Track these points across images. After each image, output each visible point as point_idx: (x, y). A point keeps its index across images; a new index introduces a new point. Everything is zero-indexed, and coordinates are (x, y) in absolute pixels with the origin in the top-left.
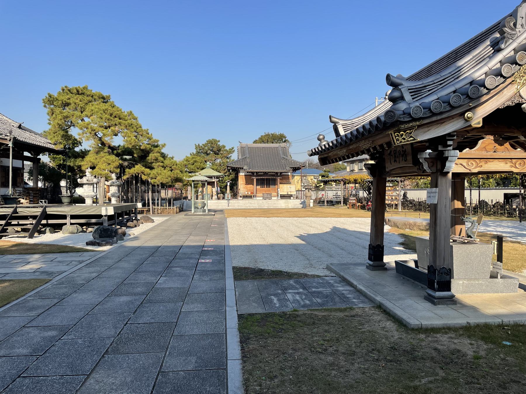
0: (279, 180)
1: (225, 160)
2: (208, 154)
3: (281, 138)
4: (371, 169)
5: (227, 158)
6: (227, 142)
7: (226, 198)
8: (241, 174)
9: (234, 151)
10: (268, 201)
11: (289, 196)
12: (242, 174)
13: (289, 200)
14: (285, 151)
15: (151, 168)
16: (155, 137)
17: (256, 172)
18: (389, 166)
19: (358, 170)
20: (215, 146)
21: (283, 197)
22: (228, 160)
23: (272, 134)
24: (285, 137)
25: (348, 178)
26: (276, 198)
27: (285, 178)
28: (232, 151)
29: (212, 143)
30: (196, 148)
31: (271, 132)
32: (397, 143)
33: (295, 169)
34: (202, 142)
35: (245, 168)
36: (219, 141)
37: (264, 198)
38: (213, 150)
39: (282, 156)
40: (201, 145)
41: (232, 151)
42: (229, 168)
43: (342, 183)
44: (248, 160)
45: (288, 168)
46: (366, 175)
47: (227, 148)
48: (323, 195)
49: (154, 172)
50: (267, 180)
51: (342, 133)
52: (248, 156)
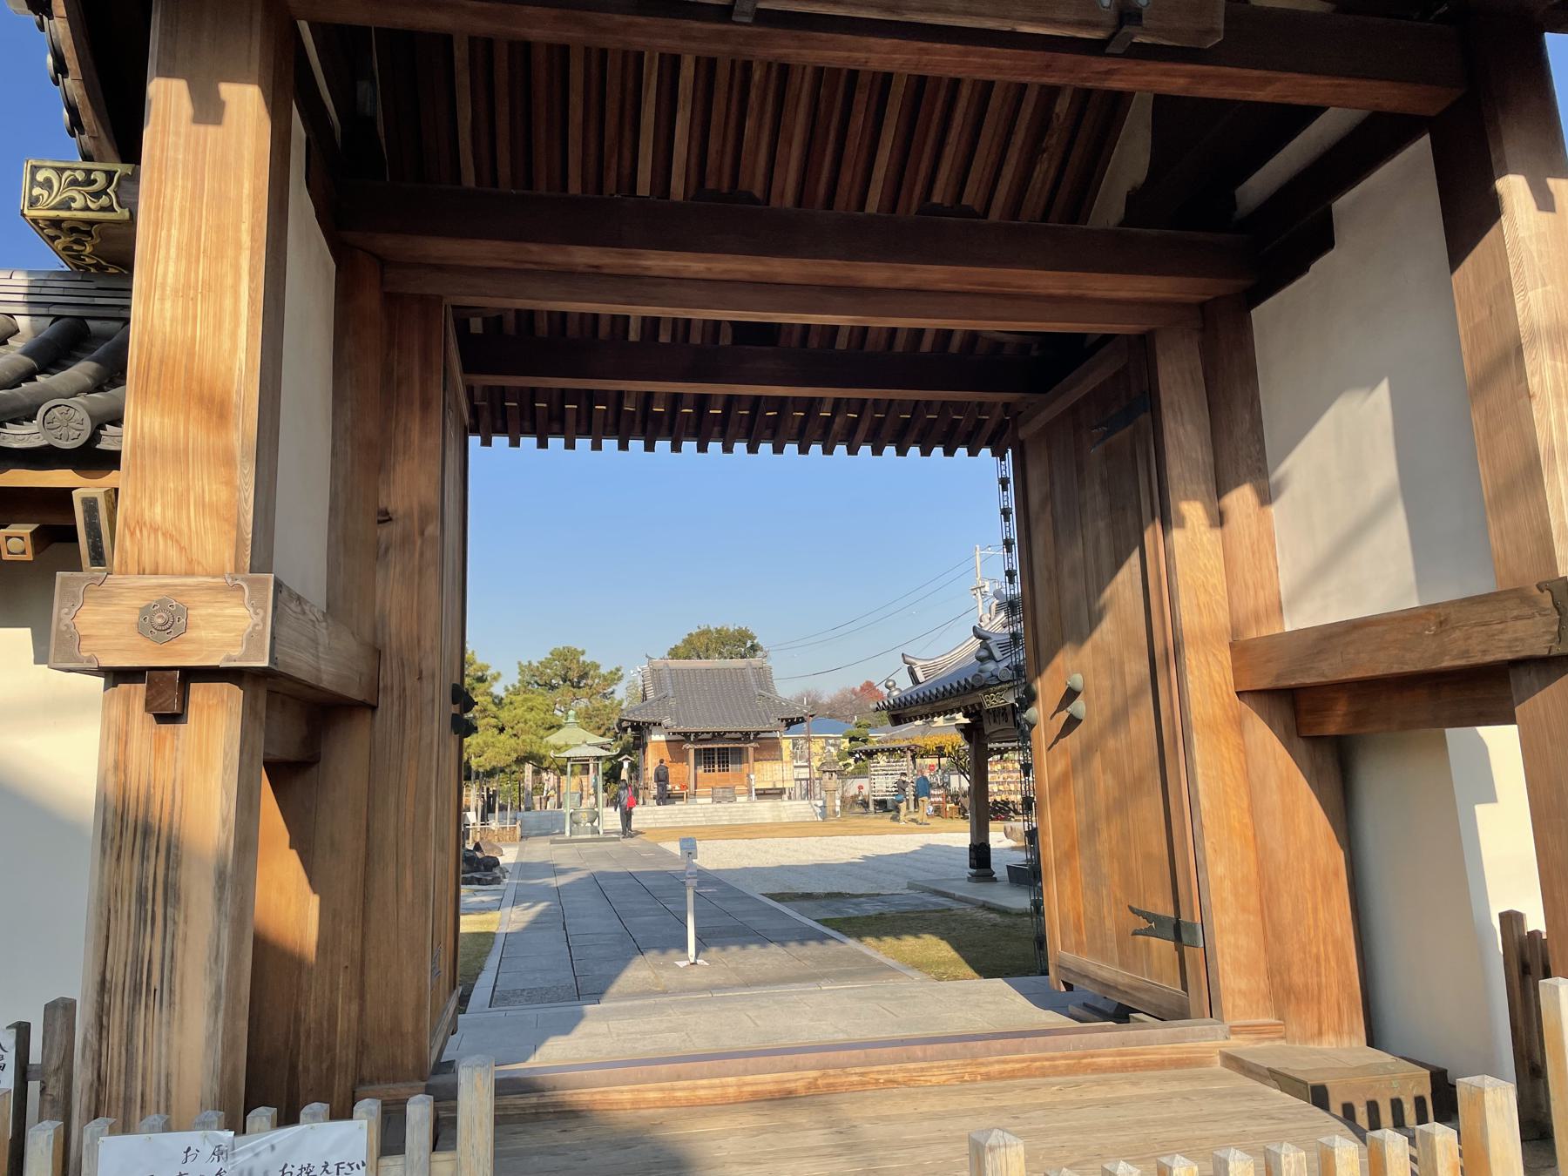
0: (751, 751)
1: (597, 702)
2: (553, 688)
3: (741, 643)
4: (966, 731)
6: (599, 655)
9: (620, 679)
10: (725, 805)
11: (777, 793)
12: (657, 737)
13: (778, 802)
17: (697, 734)
18: (989, 728)
19: (946, 729)
20: (574, 666)
21: (762, 794)
22: (607, 702)
23: (718, 631)
24: (752, 638)
25: (921, 743)
26: (744, 799)
27: (768, 747)
28: (615, 677)
29: (566, 656)
30: (522, 672)
32: (988, 707)
33: (790, 723)
35: (667, 721)
36: (583, 653)
37: (717, 800)
38: (569, 676)
40: (535, 664)
41: (615, 677)
42: (624, 724)
43: (909, 754)
44: (672, 703)
46: (959, 739)
47: (603, 671)
48: (861, 787)
50: (720, 752)
51: (921, 678)
52: (671, 693)
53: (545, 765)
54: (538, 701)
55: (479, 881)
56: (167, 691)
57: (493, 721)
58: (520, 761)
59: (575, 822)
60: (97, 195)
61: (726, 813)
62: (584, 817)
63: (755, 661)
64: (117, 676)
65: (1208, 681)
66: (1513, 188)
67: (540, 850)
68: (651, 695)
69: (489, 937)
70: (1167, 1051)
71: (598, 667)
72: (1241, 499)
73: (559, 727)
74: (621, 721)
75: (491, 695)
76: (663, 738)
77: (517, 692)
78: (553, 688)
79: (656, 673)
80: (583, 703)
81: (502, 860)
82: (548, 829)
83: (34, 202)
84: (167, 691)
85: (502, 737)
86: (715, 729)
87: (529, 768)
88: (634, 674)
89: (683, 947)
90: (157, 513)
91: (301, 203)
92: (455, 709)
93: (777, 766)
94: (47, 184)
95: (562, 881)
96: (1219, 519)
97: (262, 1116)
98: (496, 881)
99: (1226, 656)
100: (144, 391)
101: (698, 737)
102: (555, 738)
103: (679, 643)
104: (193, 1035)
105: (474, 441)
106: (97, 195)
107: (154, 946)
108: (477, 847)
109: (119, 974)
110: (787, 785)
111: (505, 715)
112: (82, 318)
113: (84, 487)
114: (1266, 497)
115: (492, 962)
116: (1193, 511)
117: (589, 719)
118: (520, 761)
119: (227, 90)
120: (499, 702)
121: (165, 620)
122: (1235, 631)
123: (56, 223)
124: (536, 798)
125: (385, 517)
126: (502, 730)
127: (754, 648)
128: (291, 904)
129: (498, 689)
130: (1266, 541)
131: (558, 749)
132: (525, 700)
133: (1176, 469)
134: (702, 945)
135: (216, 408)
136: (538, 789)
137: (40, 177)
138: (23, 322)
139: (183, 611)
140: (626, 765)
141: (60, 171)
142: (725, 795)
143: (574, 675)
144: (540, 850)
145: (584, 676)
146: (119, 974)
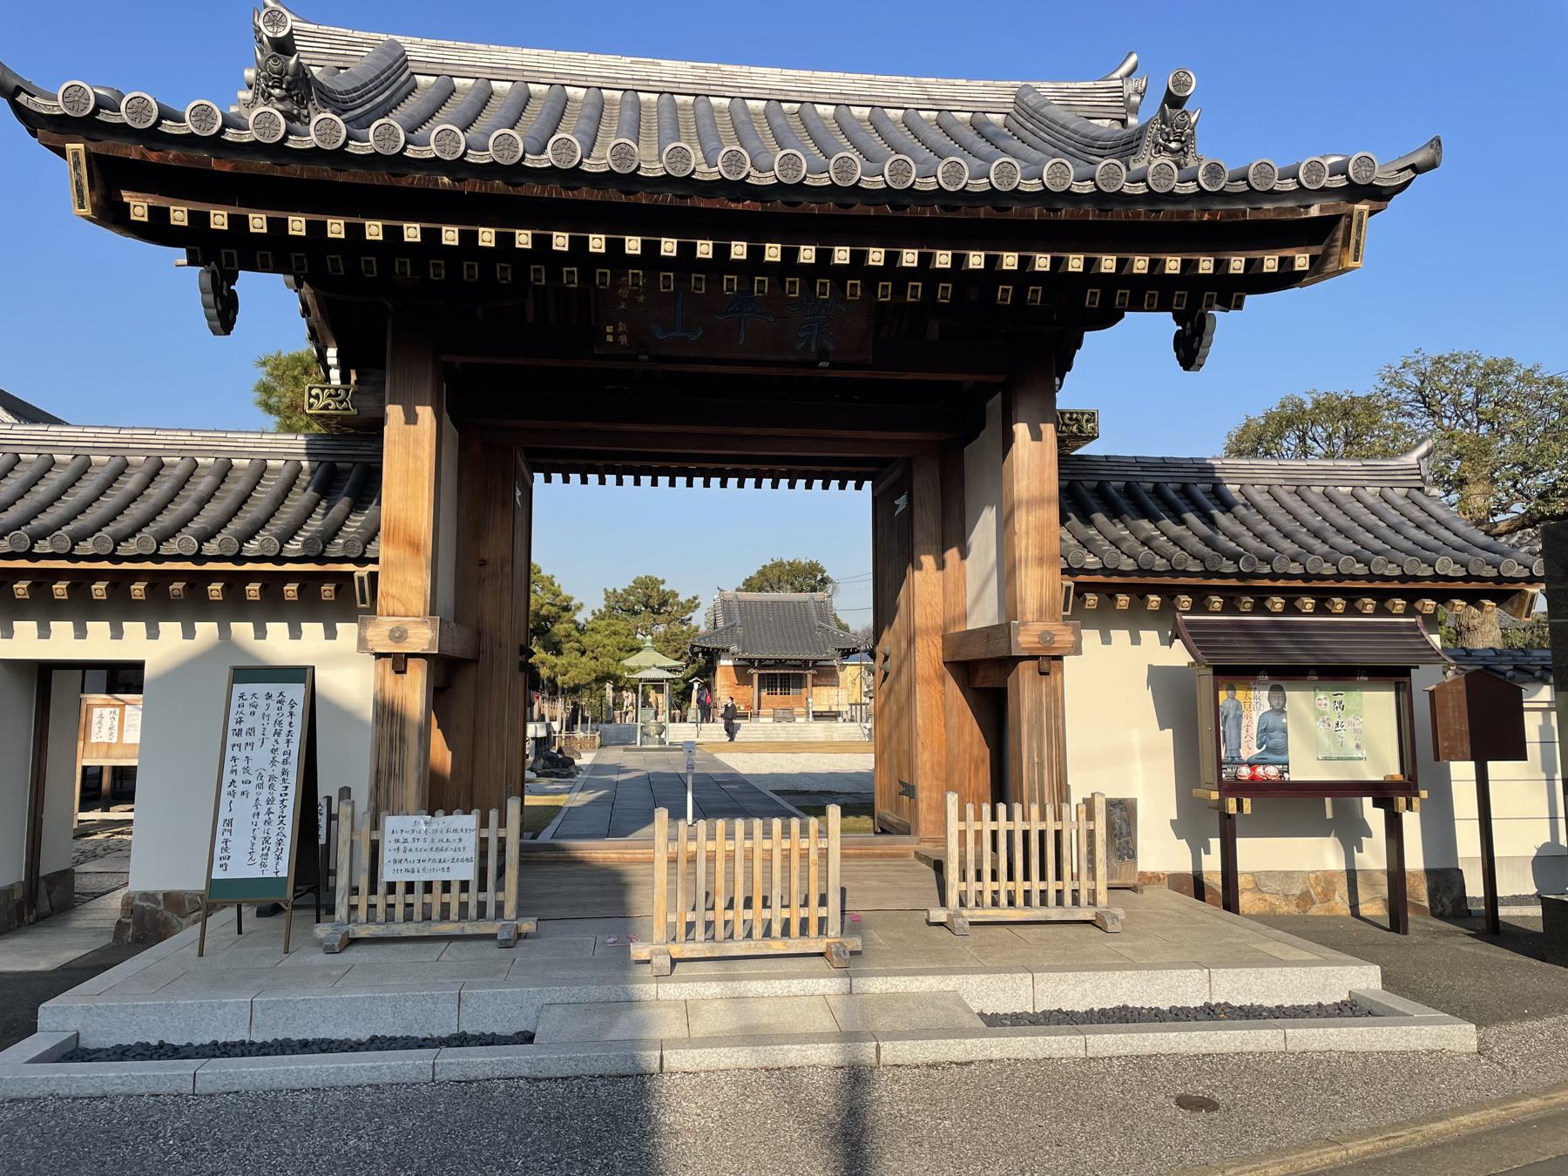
0: (809, 677)
1: (676, 628)
2: (636, 613)
5: (682, 622)
7: (689, 718)
8: (723, 662)
9: (697, 606)
10: (784, 724)
11: (833, 716)
12: (725, 663)
13: (833, 724)
14: (824, 610)
15: (559, 653)
16: (565, 592)
21: (818, 716)
26: (802, 720)
27: (826, 674)
28: (693, 604)
30: (607, 598)
31: (788, 558)
33: (846, 653)
34: (622, 583)
37: (777, 720)
38: (649, 602)
39: (818, 623)
40: (619, 591)
41: (693, 604)
44: (740, 631)
45: (831, 651)
47: (682, 599)
49: (561, 661)
50: (783, 676)
53: (621, 684)
54: (620, 626)
55: (558, 775)
56: (400, 663)
57: (576, 645)
58: (601, 679)
59: (644, 734)
60: (341, 402)
61: (783, 731)
62: (653, 730)
63: (818, 596)
64: (379, 656)
65: (928, 656)
66: (1021, 430)
67: (614, 756)
68: (720, 624)
69: (559, 808)
70: (887, 849)
71: (676, 595)
72: (952, 555)
73: (639, 650)
74: (693, 646)
75: (574, 622)
76: (730, 663)
77: (602, 617)
78: (636, 613)
79: (725, 603)
80: (661, 629)
81: (577, 762)
82: (624, 739)
83: (311, 406)
84: (400, 663)
85: (584, 659)
86: (777, 656)
87: (609, 686)
88: (708, 601)
89: (685, 817)
90: (394, 590)
91: (446, 417)
92: (522, 659)
93: (833, 691)
94: (317, 397)
95: (622, 777)
96: (941, 565)
97: (440, 812)
98: (571, 775)
99: (939, 642)
100: (387, 541)
101: (762, 663)
102: (630, 662)
103: (753, 573)
104: (411, 788)
105: (539, 477)
106: (341, 402)
107: (396, 758)
108: (560, 751)
109: (384, 768)
110: (841, 709)
111: (586, 640)
112: (333, 463)
113: (362, 572)
114: (964, 555)
115: (557, 820)
116: (928, 561)
117: (666, 644)
118: (601, 679)
119: (419, 409)
120: (581, 630)
121: (399, 635)
122: (945, 629)
123: (321, 416)
124: (617, 713)
125: (483, 563)
126: (583, 653)
127: (824, 581)
128: (441, 754)
129: (580, 617)
130: (961, 582)
131: (632, 670)
132: (609, 625)
133: (919, 535)
134: (696, 816)
135: (415, 547)
136: (618, 704)
137: (314, 392)
138: (305, 464)
139: (405, 631)
140: (696, 686)
141: (323, 390)
142: (787, 716)
143: (654, 602)
144: (614, 756)
145: (664, 603)
146: (384, 768)
